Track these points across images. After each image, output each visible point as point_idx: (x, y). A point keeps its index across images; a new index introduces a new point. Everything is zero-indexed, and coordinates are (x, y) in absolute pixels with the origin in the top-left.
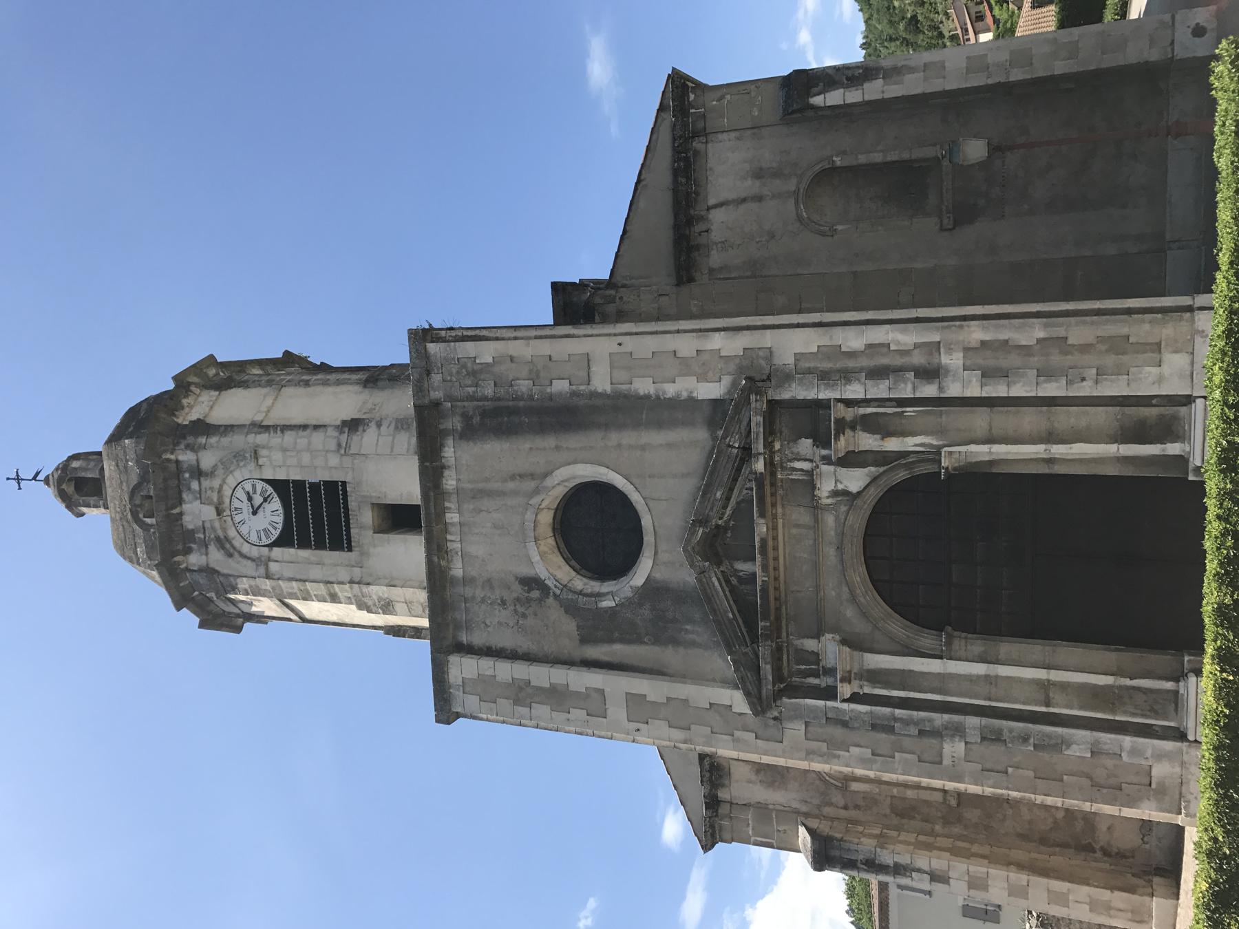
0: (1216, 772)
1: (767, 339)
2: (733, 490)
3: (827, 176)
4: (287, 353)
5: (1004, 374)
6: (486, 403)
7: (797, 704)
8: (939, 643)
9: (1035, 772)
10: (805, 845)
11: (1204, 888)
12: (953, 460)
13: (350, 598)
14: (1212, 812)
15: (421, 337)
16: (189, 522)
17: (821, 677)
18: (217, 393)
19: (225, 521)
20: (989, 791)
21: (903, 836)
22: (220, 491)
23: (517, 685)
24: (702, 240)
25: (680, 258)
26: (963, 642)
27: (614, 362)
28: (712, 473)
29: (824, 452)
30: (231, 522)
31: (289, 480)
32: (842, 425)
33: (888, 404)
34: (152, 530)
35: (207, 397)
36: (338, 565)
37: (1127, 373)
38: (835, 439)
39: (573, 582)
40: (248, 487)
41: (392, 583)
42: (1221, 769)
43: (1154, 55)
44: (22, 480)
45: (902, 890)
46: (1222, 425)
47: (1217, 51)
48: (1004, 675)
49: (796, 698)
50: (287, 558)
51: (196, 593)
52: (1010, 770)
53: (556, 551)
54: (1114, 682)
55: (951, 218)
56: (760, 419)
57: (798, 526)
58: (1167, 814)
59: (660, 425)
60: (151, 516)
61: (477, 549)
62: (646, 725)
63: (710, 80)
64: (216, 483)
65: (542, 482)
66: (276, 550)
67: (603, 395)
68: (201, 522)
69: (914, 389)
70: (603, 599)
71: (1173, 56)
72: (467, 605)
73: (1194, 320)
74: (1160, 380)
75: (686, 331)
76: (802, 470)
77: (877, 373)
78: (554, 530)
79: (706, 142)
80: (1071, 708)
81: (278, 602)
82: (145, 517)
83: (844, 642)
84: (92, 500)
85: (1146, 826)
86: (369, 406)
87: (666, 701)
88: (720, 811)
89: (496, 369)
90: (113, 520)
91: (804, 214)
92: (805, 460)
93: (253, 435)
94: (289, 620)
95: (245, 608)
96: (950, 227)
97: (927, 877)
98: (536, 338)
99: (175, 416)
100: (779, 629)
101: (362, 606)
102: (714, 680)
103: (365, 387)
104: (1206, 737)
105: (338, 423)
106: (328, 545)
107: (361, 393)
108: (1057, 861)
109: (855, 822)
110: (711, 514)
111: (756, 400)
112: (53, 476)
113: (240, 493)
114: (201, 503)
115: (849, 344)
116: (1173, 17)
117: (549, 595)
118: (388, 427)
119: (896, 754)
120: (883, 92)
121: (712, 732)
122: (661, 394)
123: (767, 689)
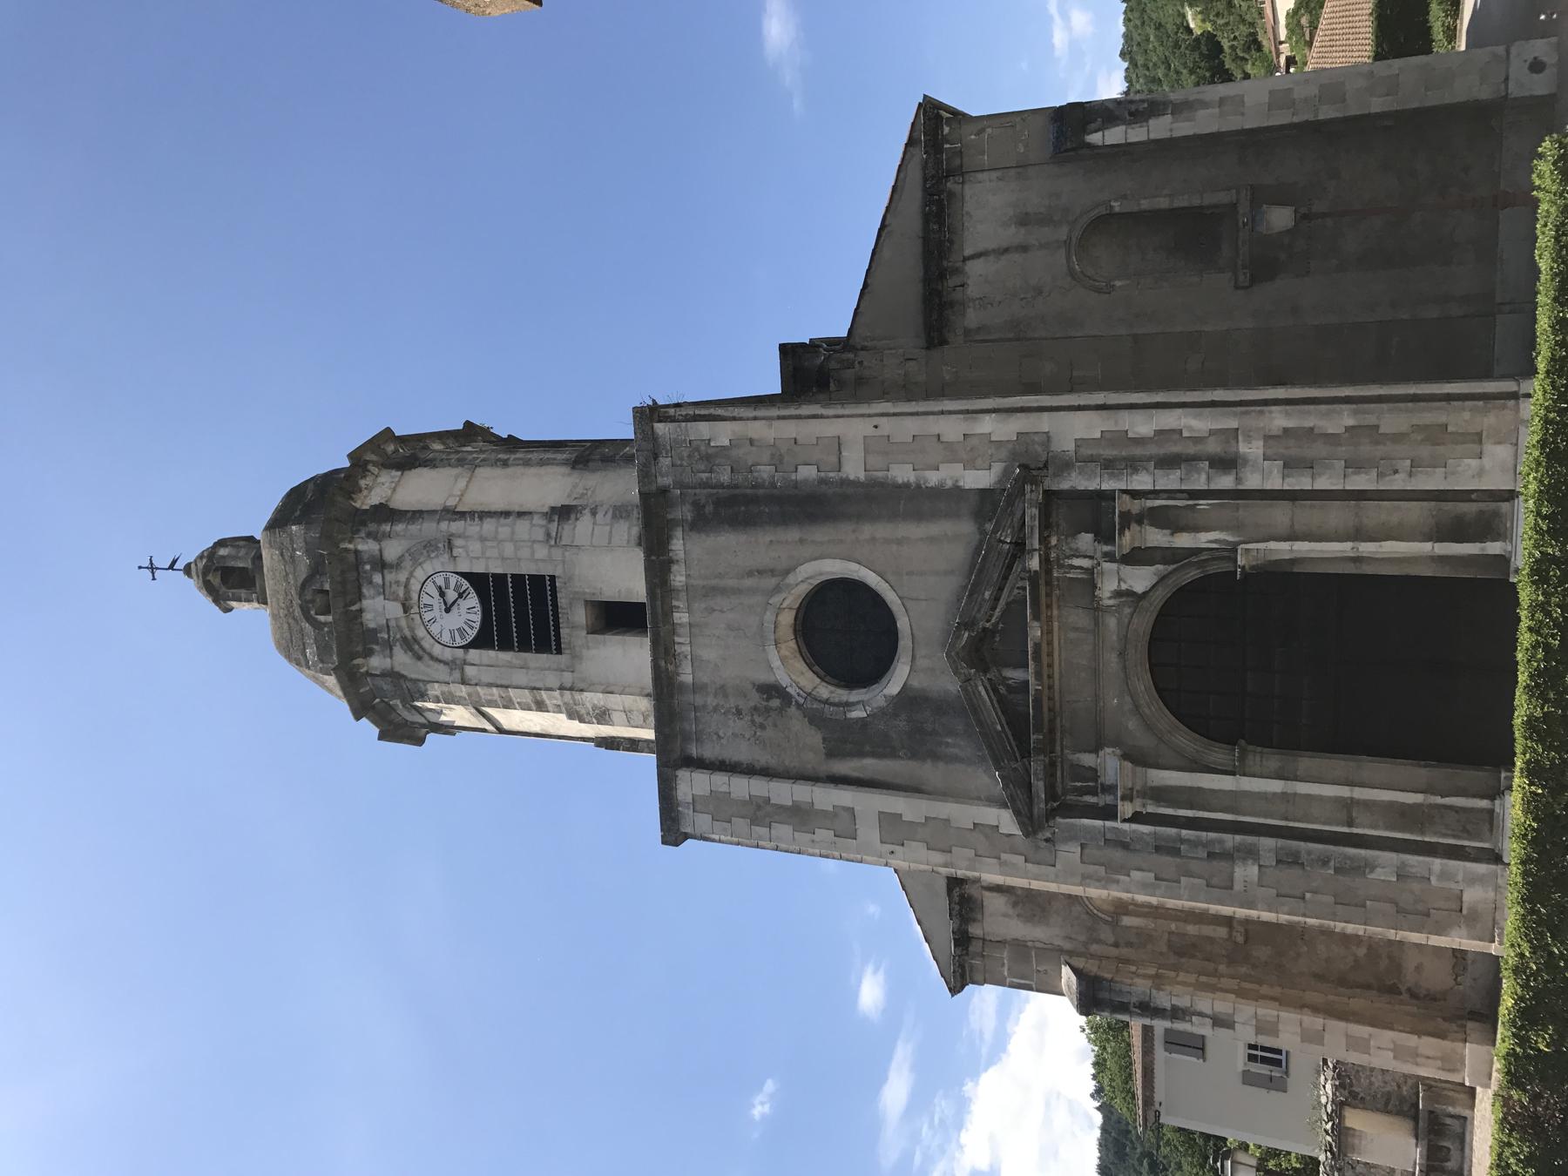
0: (1523, 887)
1: (1044, 423)
2: (1003, 590)
3: (1104, 224)
4: (468, 424)
5: (1309, 465)
6: (720, 491)
7: (1072, 825)
8: (1233, 758)
9: (1335, 896)
10: (1069, 987)
11: (1510, 1005)
12: (1251, 558)
13: (559, 706)
14: (1519, 927)
15: (648, 415)
16: (370, 620)
17: (1100, 795)
18: (399, 473)
19: (412, 619)
20: (1284, 918)
21: (1182, 977)
22: (406, 586)
23: (754, 803)
24: (957, 295)
25: (931, 317)
26: (1258, 758)
27: (868, 445)
28: (981, 571)
29: (1107, 548)
30: (420, 621)
31: (488, 574)
32: (1127, 519)
33: (1178, 495)
34: (326, 629)
35: (387, 478)
36: (546, 669)
37: (1444, 465)
38: (1119, 534)
39: (817, 690)
40: (440, 581)
41: (609, 689)
42: (1528, 883)
43: (1484, 93)
44: (157, 568)
46: (1535, 536)
47: (1540, 149)
48: (1303, 792)
49: (1071, 818)
50: (485, 661)
51: (378, 700)
52: (1308, 895)
53: (798, 655)
54: (1424, 800)
55: (1248, 275)
56: (1035, 511)
57: (1076, 629)
58: (1479, 942)
59: (919, 516)
60: (326, 612)
61: (709, 654)
62: (901, 847)
63: (974, 112)
64: (402, 577)
65: (784, 579)
66: (472, 651)
67: (855, 483)
68: (385, 621)
69: (1209, 479)
70: (852, 708)
71: (1507, 94)
72: (698, 714)
73: (1519, 408)
74: (1481, 473)
75: (950, 412)
76: (1081, 568)
77: (1168, 462)
78: (795, 631)
79: (963, 183)
80: (1375, 827)
81: (473, 711)
82: (317, 614)
83: (1125, 756)
84: (243, 593)
85: (1459, 955)
86: (580, 490)
87: (923, 821)
88: (971, 949)
89: (734, 453)
90: (274, 617)
91: (1077, 267)
92: (1085, 557)
93: (447, 522)
94: (484, 730)
95: (432, 717)
96: (1247, 284)
97: (1208, 1021)
98: (779, 418)
99: (353, 499)
100: (1053, 742)
101: (572, 715)
102: (979, 798)
103: (573, 468)
104: (1514, 851)
105: (546, 509)
106: (534, 647)
107: (569, 475)
108: (1358, 1003)
109: (1127, 961)
110: (979, 616)
111: (1032, 491)
112: (196, 565)
113: (430, 588)
114: (385, 599)
115: (1136, 429)
116: (1508, 52)
117: (791, 704)
118: (604, 515)
119: (1182, 878)
120: (1171, 130)
121: (976, 855)
122: (922, 482)
123: (1039, 808)
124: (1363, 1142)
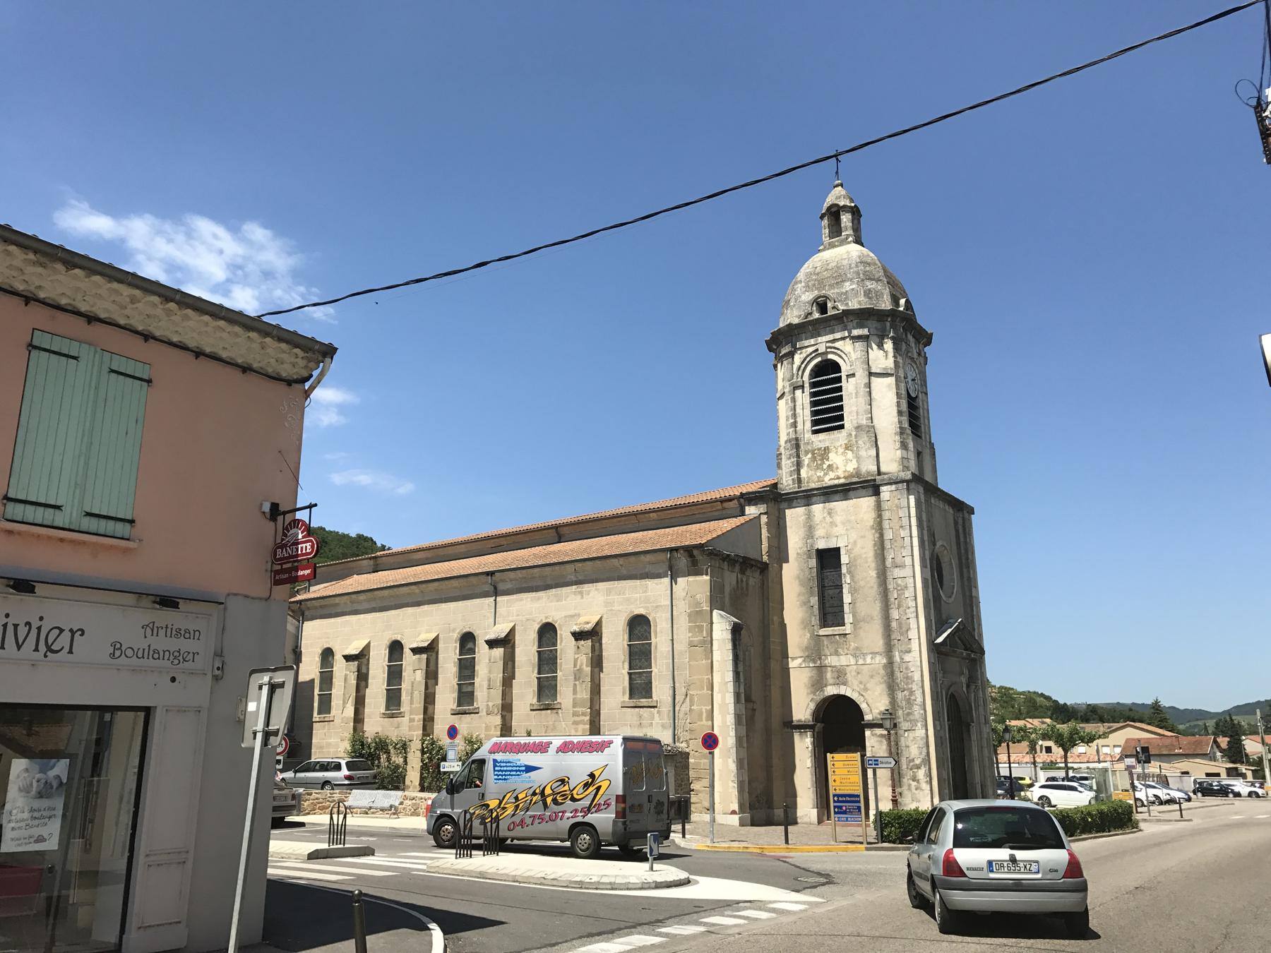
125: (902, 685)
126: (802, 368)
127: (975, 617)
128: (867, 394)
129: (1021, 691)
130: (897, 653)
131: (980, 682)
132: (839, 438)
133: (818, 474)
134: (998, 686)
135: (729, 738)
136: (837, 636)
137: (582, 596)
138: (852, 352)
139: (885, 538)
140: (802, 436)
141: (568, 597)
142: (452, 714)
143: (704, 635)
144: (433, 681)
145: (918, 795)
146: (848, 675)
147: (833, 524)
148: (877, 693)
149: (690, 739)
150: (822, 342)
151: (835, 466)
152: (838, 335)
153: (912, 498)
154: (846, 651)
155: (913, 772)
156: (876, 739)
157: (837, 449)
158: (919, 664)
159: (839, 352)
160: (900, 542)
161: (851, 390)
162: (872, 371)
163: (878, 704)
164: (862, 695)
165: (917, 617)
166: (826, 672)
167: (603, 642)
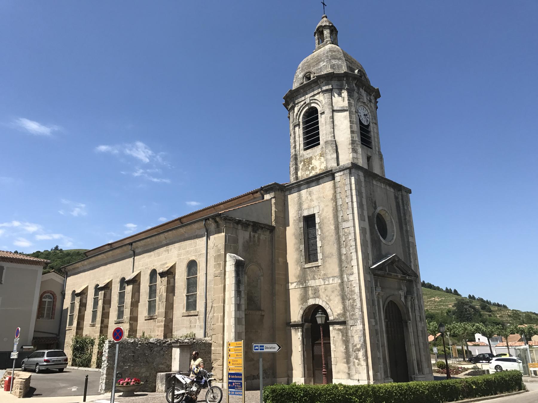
45: (4, 269)
52: (373, 337)
124: (186, 353)
125: (349, 296)
126: (298, 114)
127: (411, 254)
128: (331, 123)
129: (523, 311)
130: (345, 276)
131: (415, 294)
132: (317, 150)
133: (307, 173)
134: (511, 310)
135: (232, 333)
136: (314, 268)
137: (168, 252)
138: (323, 100)
139: (338, 205)
140: (299, 153)
141: (162, 254)
142: (115, 324)
143: (221, 269)
144: (109, 306)
145: (359, 369)
146: (320, 292)
147: (312, 200)
148: (336, 302)
149: (213, 335)
150: (307, 98)
151: (315, 167)
152: (316, 92)
153: (353, 179)
154: (319, 277)
155: (356, 353)
156: (336, 332)
157: (316, 157)
158: (358, 282)
159: (316, 101)
160: (346, 206)
161: (323, 121)
162: (334, 109)
163: (336, 309)
164: (328, 304)
165: (356, 251)
166: (308, 291)
167: (176, 278)
